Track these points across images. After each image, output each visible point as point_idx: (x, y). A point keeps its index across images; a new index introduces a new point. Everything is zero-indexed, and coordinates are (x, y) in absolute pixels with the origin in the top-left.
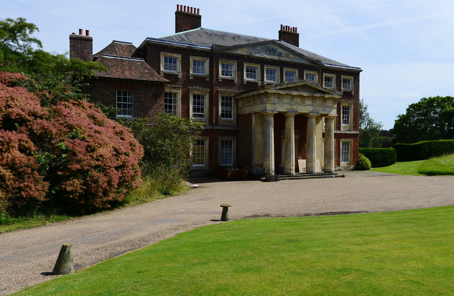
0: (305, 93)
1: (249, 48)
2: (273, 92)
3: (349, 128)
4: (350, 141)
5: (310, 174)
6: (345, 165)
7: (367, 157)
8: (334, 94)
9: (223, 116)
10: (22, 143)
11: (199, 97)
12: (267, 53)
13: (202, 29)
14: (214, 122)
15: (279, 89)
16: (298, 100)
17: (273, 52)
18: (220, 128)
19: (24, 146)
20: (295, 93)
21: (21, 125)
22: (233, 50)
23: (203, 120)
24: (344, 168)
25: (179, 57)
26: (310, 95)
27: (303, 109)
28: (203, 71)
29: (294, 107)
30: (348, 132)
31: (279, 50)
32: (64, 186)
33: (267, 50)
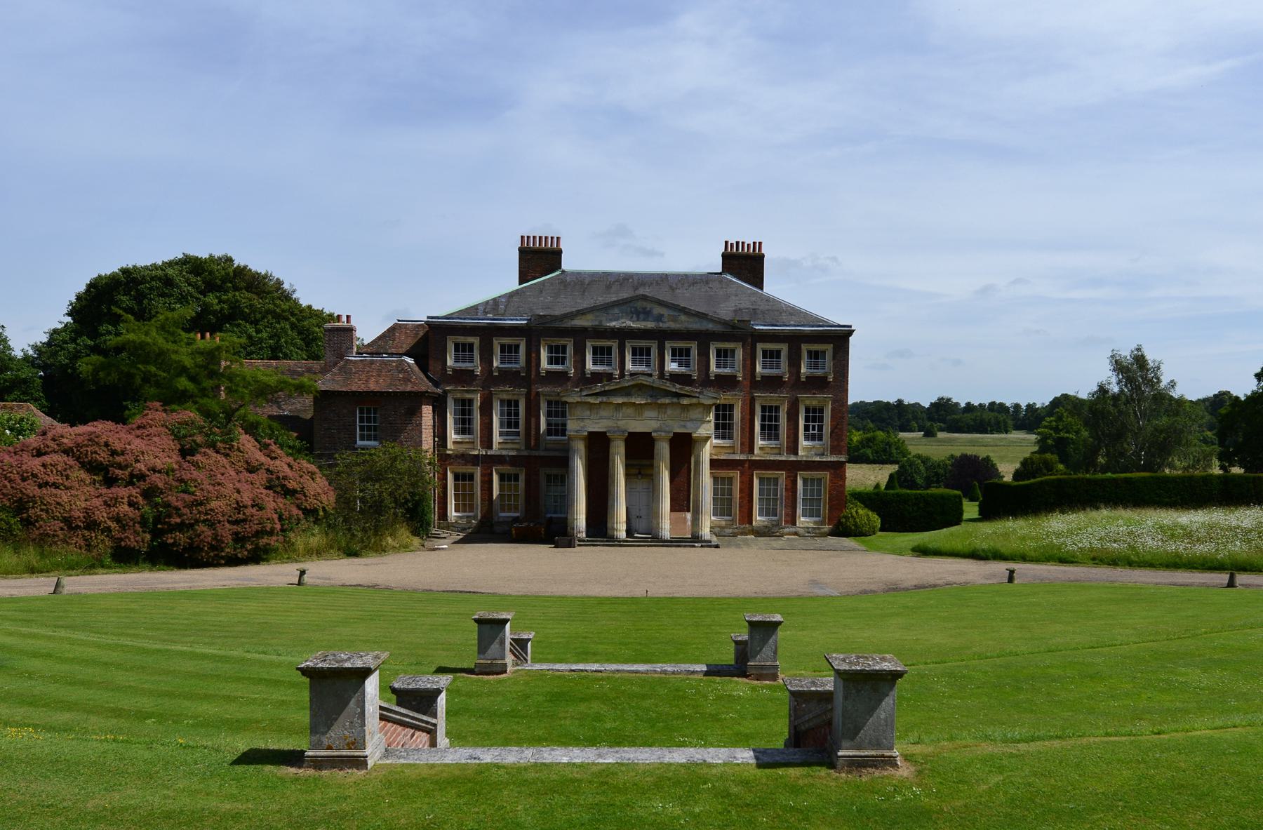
0: (639, 399)
1: (598, 314)
2: (575, 401)
3: (822, 449)
4: (823, 476)
5: (695, 540)
6: (811, 525)
7: (873, 510)
8: (701, 396)
9: (549, 432)
10: (132, 498)
11: (509, 403)
12: (632, 317)
13: (563, 271)
14: (533, 443)
15: (586, 395)
16: (630, 411)
17: (646, 314)
18: (542, 454)
19: (133, 500)
20: (620, 400)
21: (138, 481)
22: (567, 320)
23: (517, 441)
24: (806, 530)
25: (476, 341)
26: (649, 401)
27: (638, 426)
28: (517, 361)
29: (619, 423)
30: (818, 459)
31: (658, 310)
32: (164, 539)
33: (631, 312)
